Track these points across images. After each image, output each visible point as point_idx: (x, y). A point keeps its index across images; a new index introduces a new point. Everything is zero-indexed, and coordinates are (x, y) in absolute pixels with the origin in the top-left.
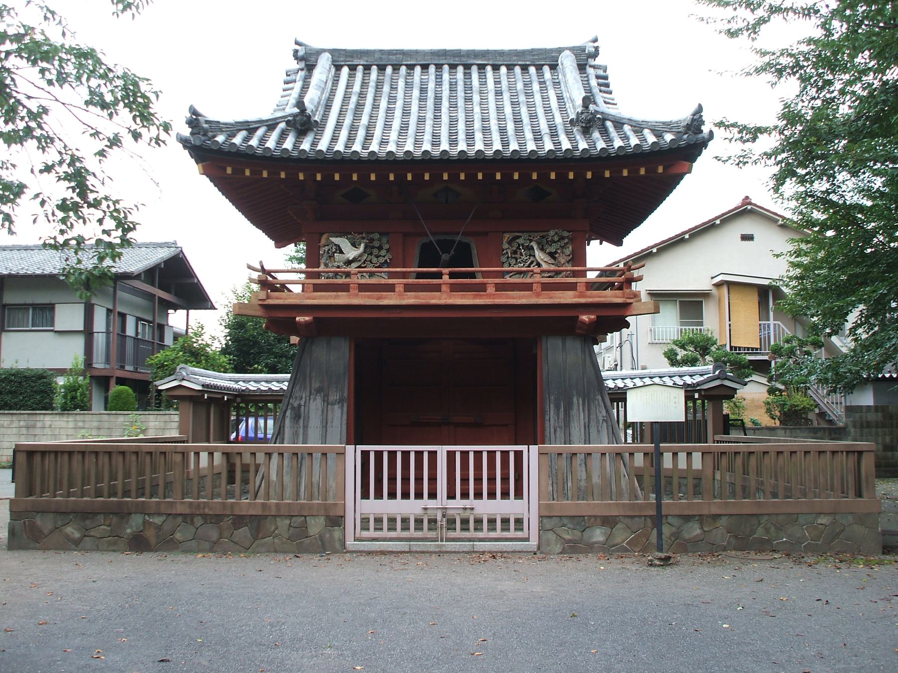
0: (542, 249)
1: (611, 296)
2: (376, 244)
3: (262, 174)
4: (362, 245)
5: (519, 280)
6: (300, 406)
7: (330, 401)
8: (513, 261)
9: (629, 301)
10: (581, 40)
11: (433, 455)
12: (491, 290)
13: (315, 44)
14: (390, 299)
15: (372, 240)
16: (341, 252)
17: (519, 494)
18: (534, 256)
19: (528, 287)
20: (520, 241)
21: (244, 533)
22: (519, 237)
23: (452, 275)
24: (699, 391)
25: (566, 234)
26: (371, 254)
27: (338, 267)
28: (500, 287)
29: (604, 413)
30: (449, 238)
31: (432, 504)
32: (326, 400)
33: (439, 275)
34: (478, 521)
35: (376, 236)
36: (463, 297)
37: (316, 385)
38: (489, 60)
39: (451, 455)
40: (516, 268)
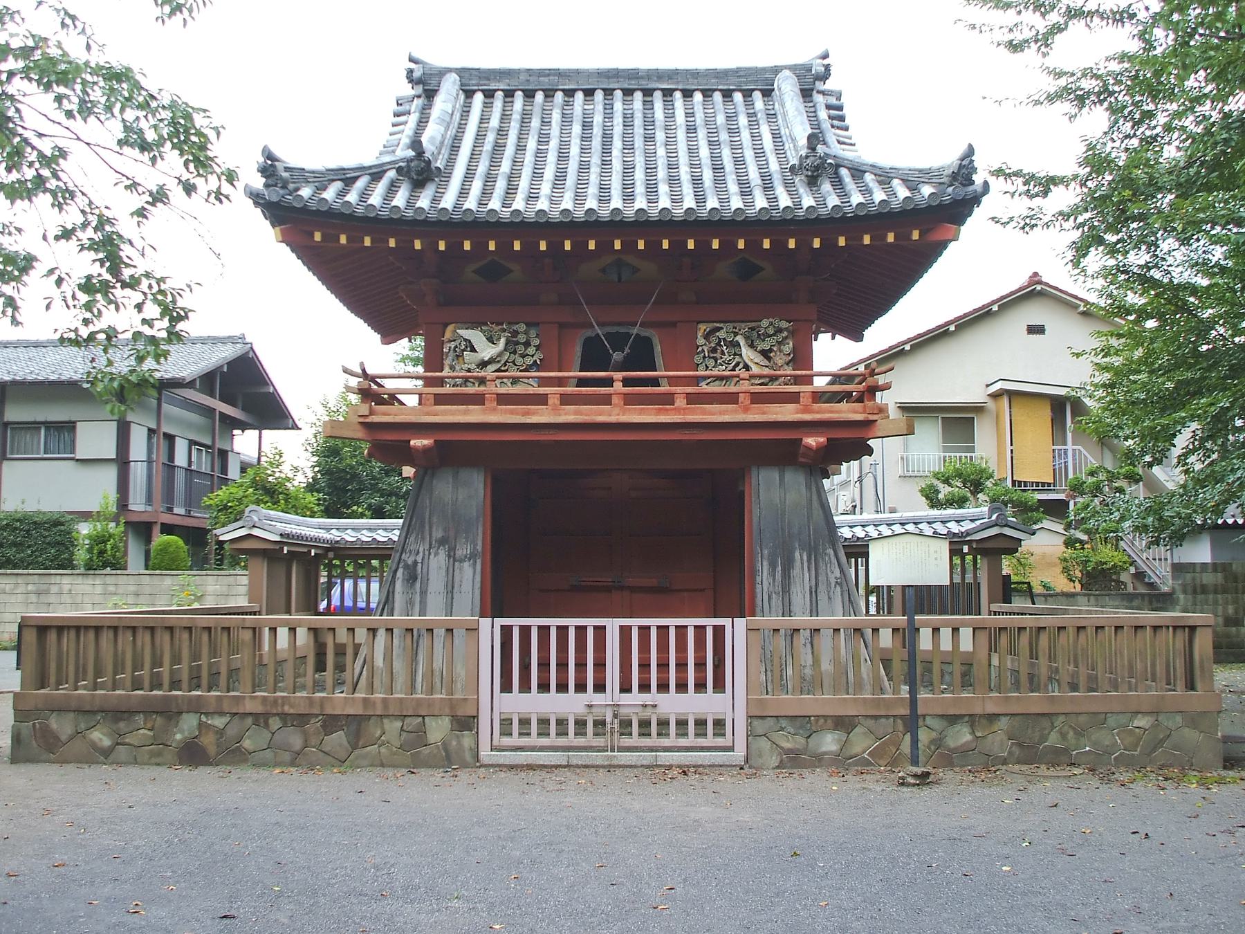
0: (752, 346)
1: (847, 411)
2: (522, 338)
4: (503, 341)
8: (711, 363)
9: (872, 417)
12: (680, 402)
14: (541, 415)
16: (473, 350)
17: (719, 685)
20: (721, 334)
21: (338, 739)
22: (719, 329)
23: (627, 382)
25: (784, 324)
26: (514, 352)
27: (469, 371)
28: (692, 399)
30: (622, 330)
31: (598, 699)
32: (451, 555)
33: (609, 382)
34: (664, 723)
35: (522, 327)
37: (438, 534)
39: (625, 632)
40: (715, 372)
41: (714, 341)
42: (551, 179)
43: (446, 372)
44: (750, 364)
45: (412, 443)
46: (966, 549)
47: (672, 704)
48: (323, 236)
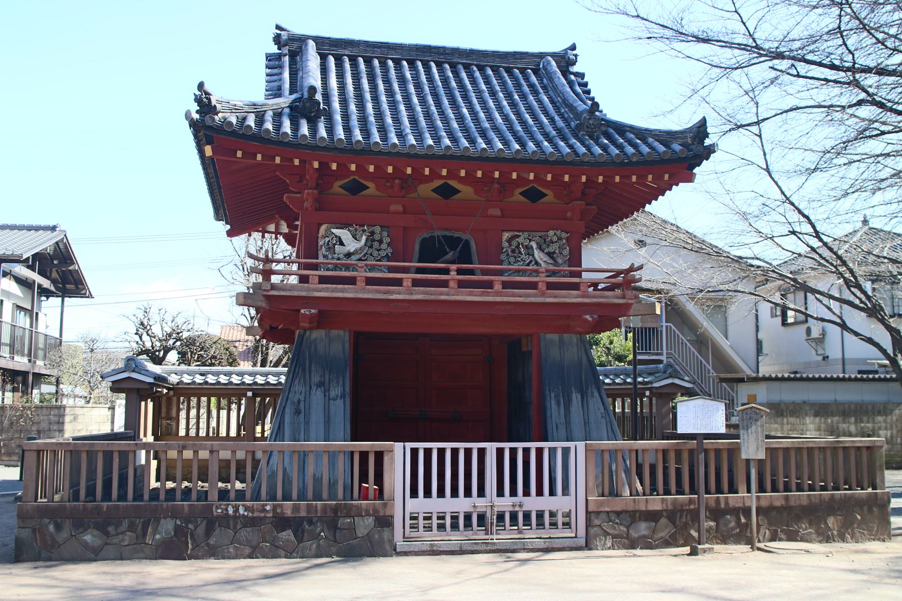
0: (540, 248)
1: (613, 298)
2: (377, 237)
3: (274, 161)
4: (364, 238)
5: (517, 279)
6: (299, 401)
7: (331, 396)
8: (512, 260)
9: (630, 301)
10: (558, 48)
11: (482, 452)
12: (498, 287)
13: (297, 28)
14: (397, 294)
15: (372, 233)
16: (342, 244)
17: (566, 491)
18: (533, 255)
19: (533, 286)
20: (520, 240)
21: (287, 535)
22: (519, 236)
23: (459, 272)
24: (650, 389)
25: (564, 235)
26: (371, 247)
27: (339, 259)
28: (506, 285)
29: (602, 410)
30: (456, 235)
31: (481, 503)
32: (326, 392)
33: (446, 271)
34: (527, 516)
35: (377, 229)
36: (470, 294)
37: (316, 379)
38: (473, 60)
39: (500, 452)
40: (516, 267)
41: (514, 243)
42: (402, 123)
43: (321, 260)
44: (540, 261)
45: (302, 311)
46: (647, 393)
47: (533, 503)
48: (293, 162)
